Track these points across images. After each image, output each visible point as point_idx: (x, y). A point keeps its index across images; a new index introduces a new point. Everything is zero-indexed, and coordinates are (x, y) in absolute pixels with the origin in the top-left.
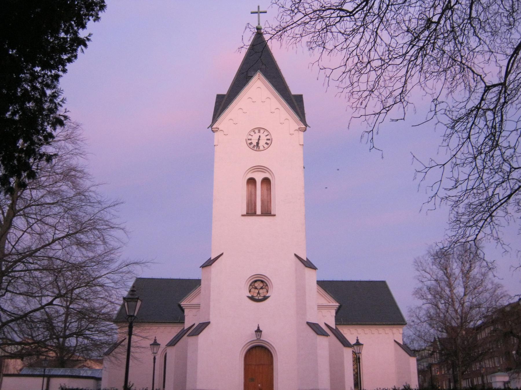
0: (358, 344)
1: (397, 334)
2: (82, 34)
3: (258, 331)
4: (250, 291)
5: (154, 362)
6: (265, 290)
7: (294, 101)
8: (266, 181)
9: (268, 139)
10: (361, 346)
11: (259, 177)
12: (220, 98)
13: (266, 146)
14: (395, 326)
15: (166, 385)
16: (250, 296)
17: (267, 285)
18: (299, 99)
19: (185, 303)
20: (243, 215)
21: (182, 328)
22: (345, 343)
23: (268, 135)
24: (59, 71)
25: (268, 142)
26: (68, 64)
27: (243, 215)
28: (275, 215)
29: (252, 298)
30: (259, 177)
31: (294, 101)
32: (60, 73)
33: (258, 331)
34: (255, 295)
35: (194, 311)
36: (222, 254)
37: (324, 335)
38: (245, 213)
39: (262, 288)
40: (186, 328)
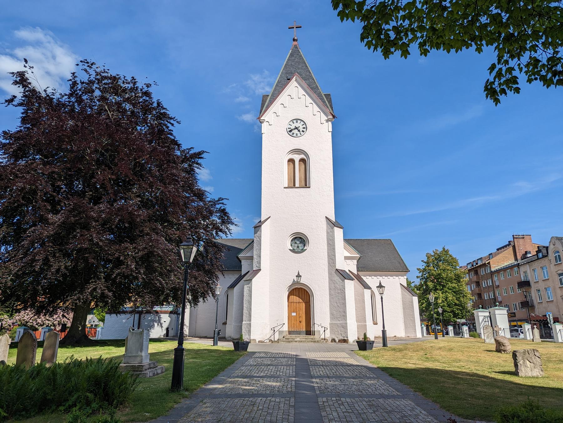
0: (380, 286)
1: (403, 280)
3: (299, 276)
5: (382, 301)
9: (304, 128)
11: (297, 158)
18: (328, 96)
22: (366, 287)
26: (363, 24)
29: (293, 251)
33: (299, 276)
34: (295, 248)
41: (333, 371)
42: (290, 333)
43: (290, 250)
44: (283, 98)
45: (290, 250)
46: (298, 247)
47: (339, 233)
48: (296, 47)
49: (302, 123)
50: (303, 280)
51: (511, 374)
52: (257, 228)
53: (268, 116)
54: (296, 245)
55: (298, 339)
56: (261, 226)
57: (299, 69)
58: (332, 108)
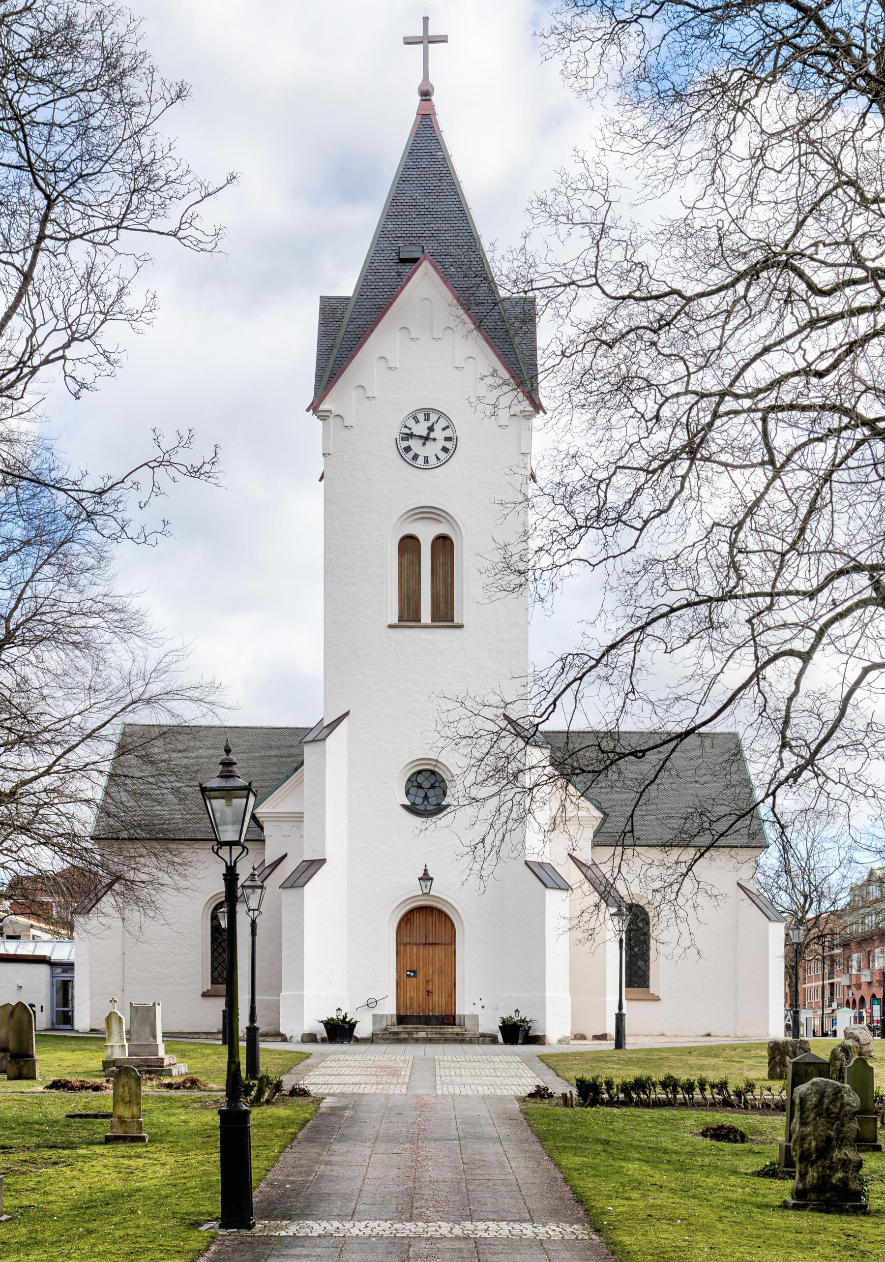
3: (426, 877)
4: (407, 793)
6: (439, 791)
11: (426, 534)
12: (331, 311)
13: (443, 456)
15: (258, 932)
20: (390, 626)
23: (448, 427)
25: (449, 445)
27: (390, 626)
28: (461, 626)
29: (412, 809)
30: (426, 534)
33: (426, 877)
34: (419, 801)
35: (286, 827)
36: (347, 714)
37: (560, 888)
38: (395, 620)
39: (432, 787)
42: (401, 1019)
43: (404, 806)
45: (404, 806)
46: (426, 797)
50: (438, 889)
51: (645, 956)
54: (421, 793)
55: (422, 1035)
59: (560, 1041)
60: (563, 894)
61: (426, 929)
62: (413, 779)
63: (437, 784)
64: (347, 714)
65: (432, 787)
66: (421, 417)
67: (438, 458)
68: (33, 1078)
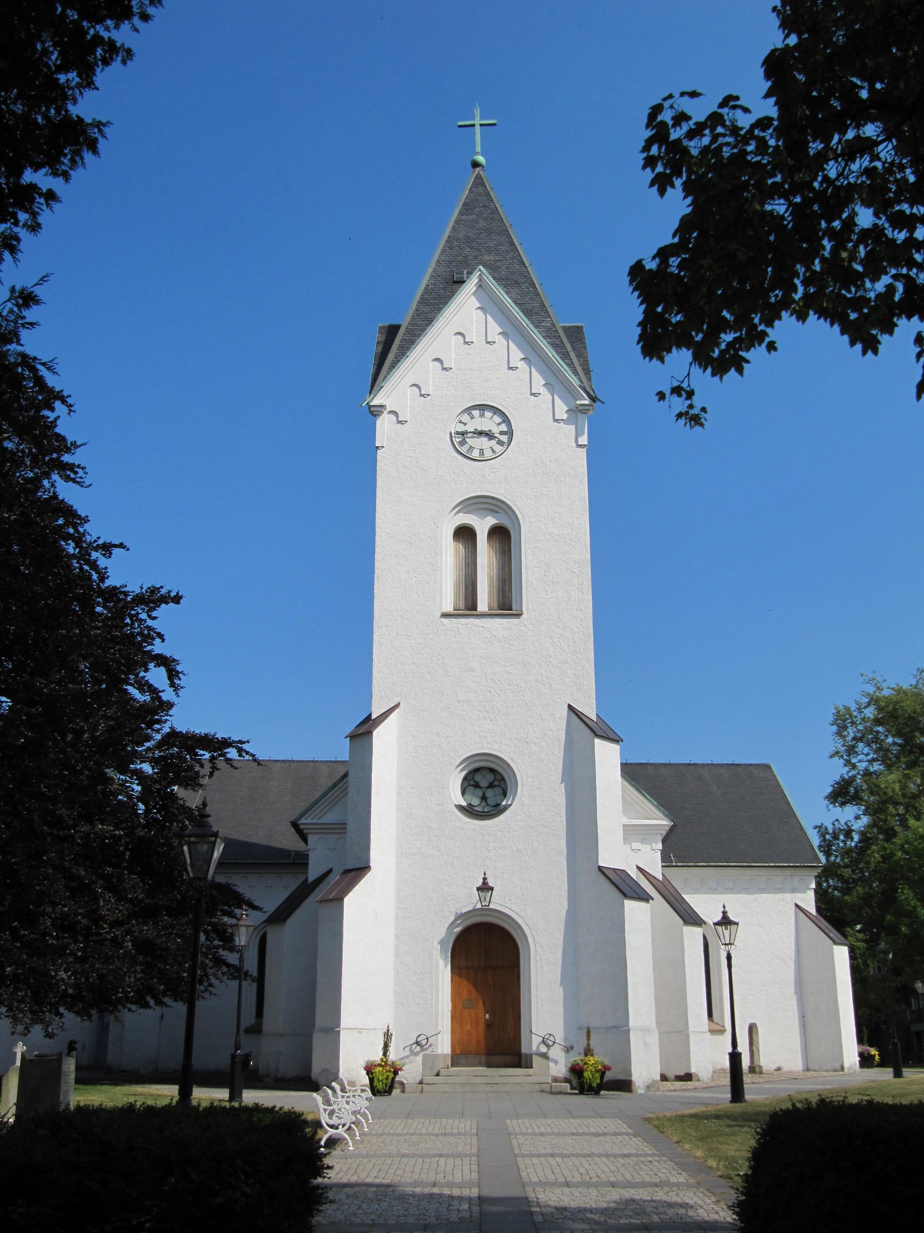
0: (725, 921)
2: (85, 107)
3: (485, 888)
4: (463, 793)
6: (498, 790)
7: (565, 340)
8: (502, 535)
10: (733, 927)
11: (482, 525)
14: (799, 872)
16: (464, 804)
17: (503, 779)
19: (309, 821)
20: (445, 615)
21: (301, 879)
22: (691, 918)
24: (16, 224)
27: (445, 615)
31: (565, 340)
32: (23, 233)
33: (485, 888)
36: (397, 706)
39: (491, 786)
40: (312, 877)
41: (582, 1170)
44: (439, 339)
45: (460, 808)
47: (607, 758)
48: (478, 177)
49: (497, 419)
50: (498, 902)
52: (363, 731)
53: (394, 393)
56: (369, 733)
57: (489, 251)
58: (587, 372)
59: (648, 1087)
60: (642, 904)
61: (486, 954)
62: (470, 777)
63: (496, 783)
64: (397, 706)
65: (491, 786)
66: (504, 438)
67: (493, 451)
68: (532, 1067)
